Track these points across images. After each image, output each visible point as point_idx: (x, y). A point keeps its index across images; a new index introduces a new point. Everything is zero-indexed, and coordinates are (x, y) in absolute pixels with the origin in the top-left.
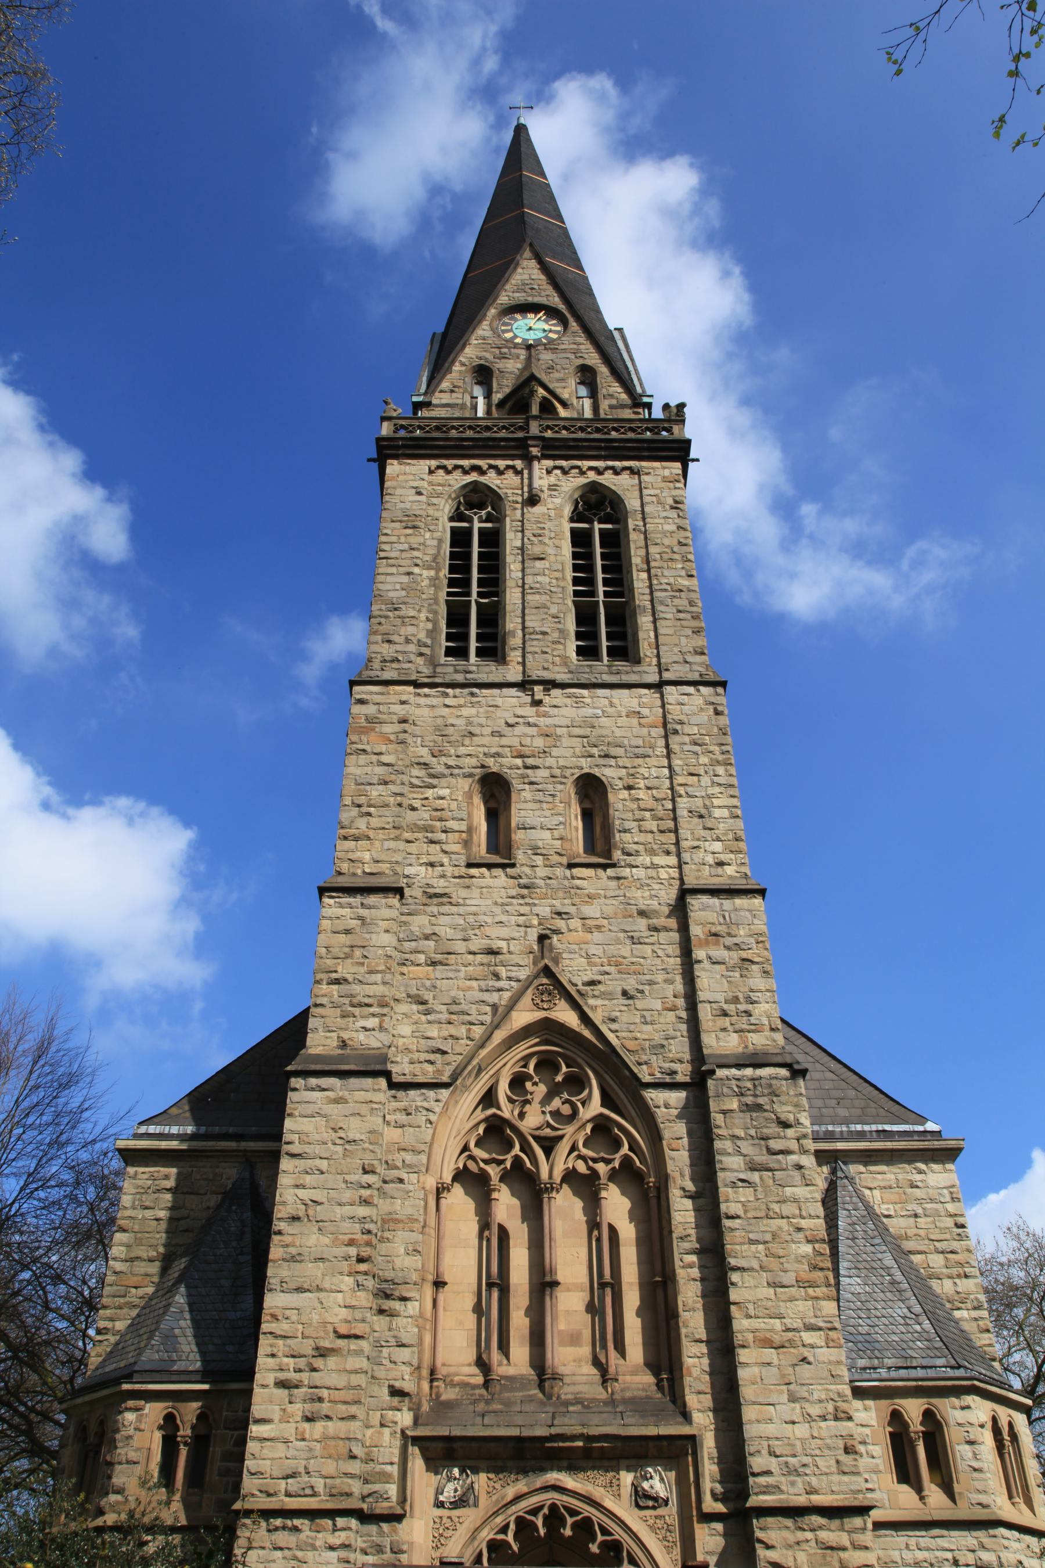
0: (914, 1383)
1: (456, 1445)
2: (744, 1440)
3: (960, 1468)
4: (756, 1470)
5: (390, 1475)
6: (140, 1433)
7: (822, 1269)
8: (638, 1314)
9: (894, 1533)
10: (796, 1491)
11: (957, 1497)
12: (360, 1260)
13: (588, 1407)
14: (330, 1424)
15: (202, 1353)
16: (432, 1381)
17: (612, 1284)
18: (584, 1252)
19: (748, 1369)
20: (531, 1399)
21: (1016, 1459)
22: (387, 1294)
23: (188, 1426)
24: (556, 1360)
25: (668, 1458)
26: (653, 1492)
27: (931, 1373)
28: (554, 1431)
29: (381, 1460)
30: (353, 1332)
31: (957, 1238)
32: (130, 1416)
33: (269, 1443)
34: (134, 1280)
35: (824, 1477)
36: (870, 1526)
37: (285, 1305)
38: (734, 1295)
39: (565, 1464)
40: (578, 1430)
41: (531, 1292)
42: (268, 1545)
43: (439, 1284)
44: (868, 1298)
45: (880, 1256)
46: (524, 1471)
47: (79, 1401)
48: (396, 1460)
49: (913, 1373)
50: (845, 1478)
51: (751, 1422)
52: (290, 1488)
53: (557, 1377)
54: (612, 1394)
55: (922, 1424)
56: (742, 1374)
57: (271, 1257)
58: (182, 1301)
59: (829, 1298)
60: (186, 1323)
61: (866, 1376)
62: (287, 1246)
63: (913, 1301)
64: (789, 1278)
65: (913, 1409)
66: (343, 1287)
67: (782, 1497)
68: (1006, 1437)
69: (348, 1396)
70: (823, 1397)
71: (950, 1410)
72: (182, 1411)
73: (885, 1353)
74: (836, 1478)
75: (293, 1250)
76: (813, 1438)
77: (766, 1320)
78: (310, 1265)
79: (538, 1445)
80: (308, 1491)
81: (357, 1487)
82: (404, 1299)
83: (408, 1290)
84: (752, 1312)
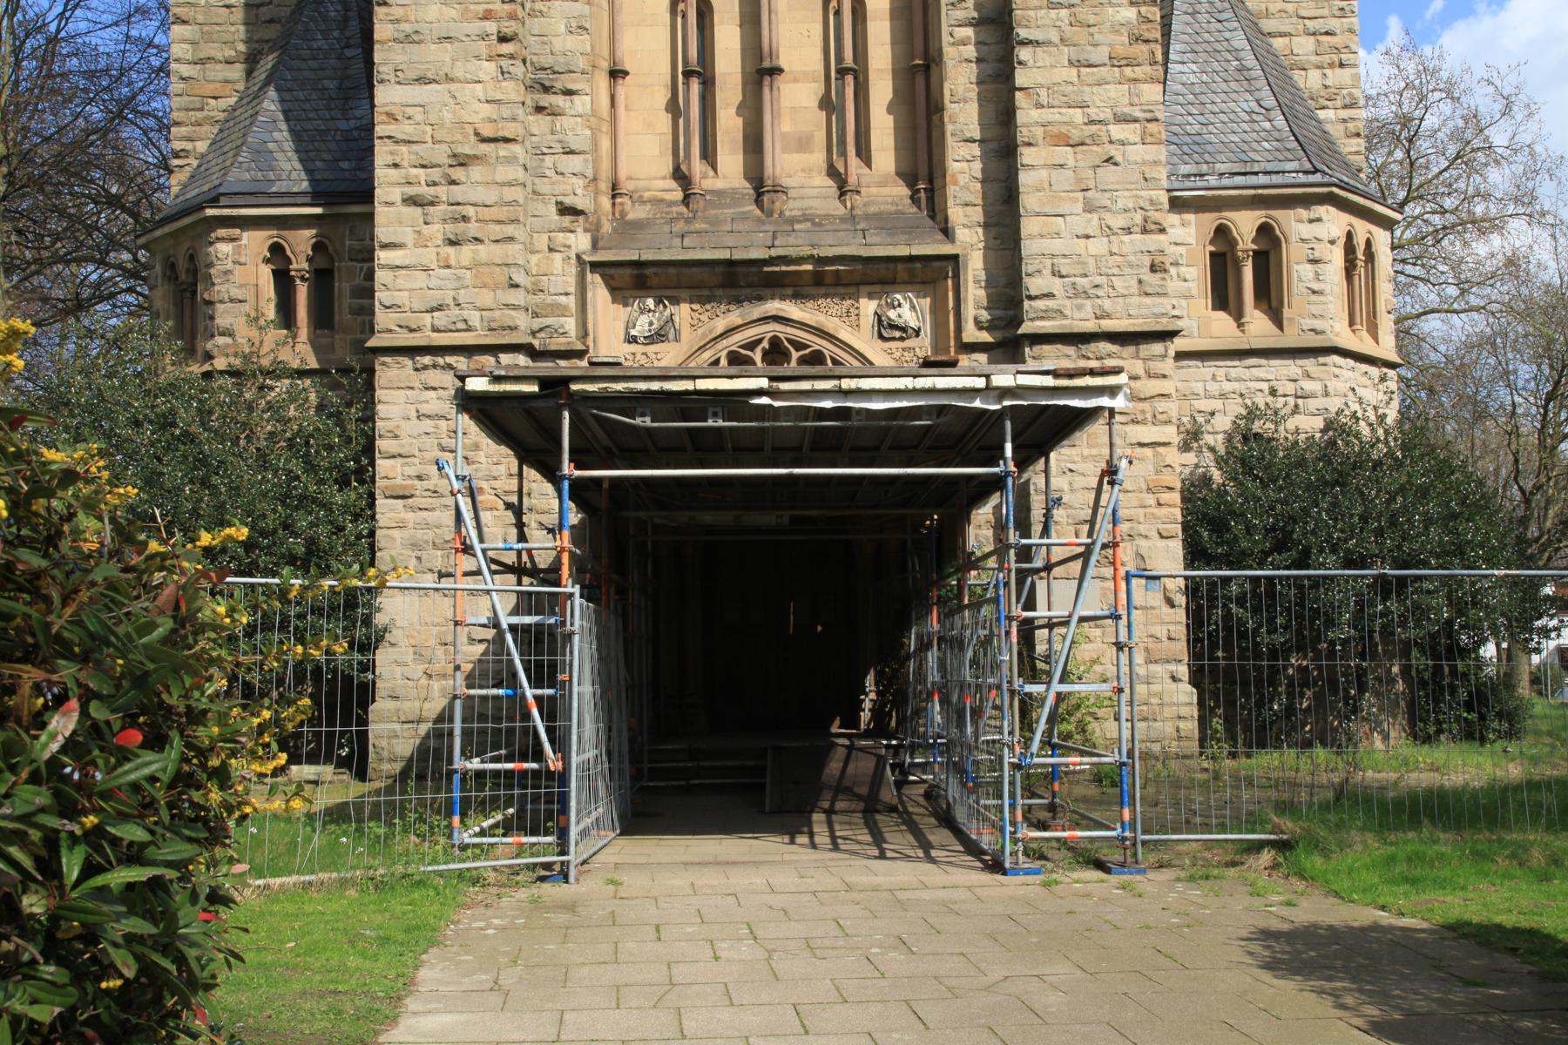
0: (1252, 192)
1: (649, 271)
2: (1021, 259)
3: (1295, 290)
4: (1033, 293)
5: (566, 308)
6: (241, 268)
7: (1147, 41)
8: (889, 111)
9: (1199, 364)
10: (1082, 316)
11: (1285, 323)
12: (503, 39)
13: (820, 224)
14: (480, 247)
15: (309, 172)
16: (614, 197)
17: (855, 71)
18: (817, 29)
19: (1032, 173)
20: (745, 217)
21: (1367, 284)
22: (545, 87)
23: (302, 258)
24: (778, 170)
25: (924, 283)
26: (900, 322)
27: (1275, 179)
28: (774, 253)
29: (552, 290)
30: (501, 134)
31: (1338, 13)
32: (224, 248)
33: (404, 272)
34: (210, 89)
35: (1120, 300)
36: (1172, 353)
37: (404, 100)
38: (1021, 78)
39: (789, 291)
40: (806, 251)
41: (744, 84)
42: (417, 384)
43: (616, 74)
44: (1204, 89)
45: (1227, 35)
46: (739, 301)
47: (158, 233)
48: (572, 289)
49: (1252, 180)
50: (1148, 300)
51: (1032, 237)
52: (436, 322)
53: (778, 190)
54: (852, 208)
55: (1253, 241)
56: (1024, 178)
57: (376, 37)
58: (273, 108)
59: (1153, 80)
60: (282, 134)
61: (1188, 184)
62: (398, 21)
63: (1266, 93)
64: (1100, 55)
65: (1245, 224)
66: (483, 76)
67: (1065, 322)
68: (1360, 255)
69: (503, 213)
70: (1131, 205)
71: (1294, 225)
72: (291, 240)
73: (1218, 157)
74: (1135, 300)
75: (407, 28)
76: (1112, 254)
77: (1063, 110)
78: (433, 47)
79: (753, 269)
80: (461, 326)
81: (523, 321)
82: (569, 93)
83: (574, 81)
84: (1044, 100)
